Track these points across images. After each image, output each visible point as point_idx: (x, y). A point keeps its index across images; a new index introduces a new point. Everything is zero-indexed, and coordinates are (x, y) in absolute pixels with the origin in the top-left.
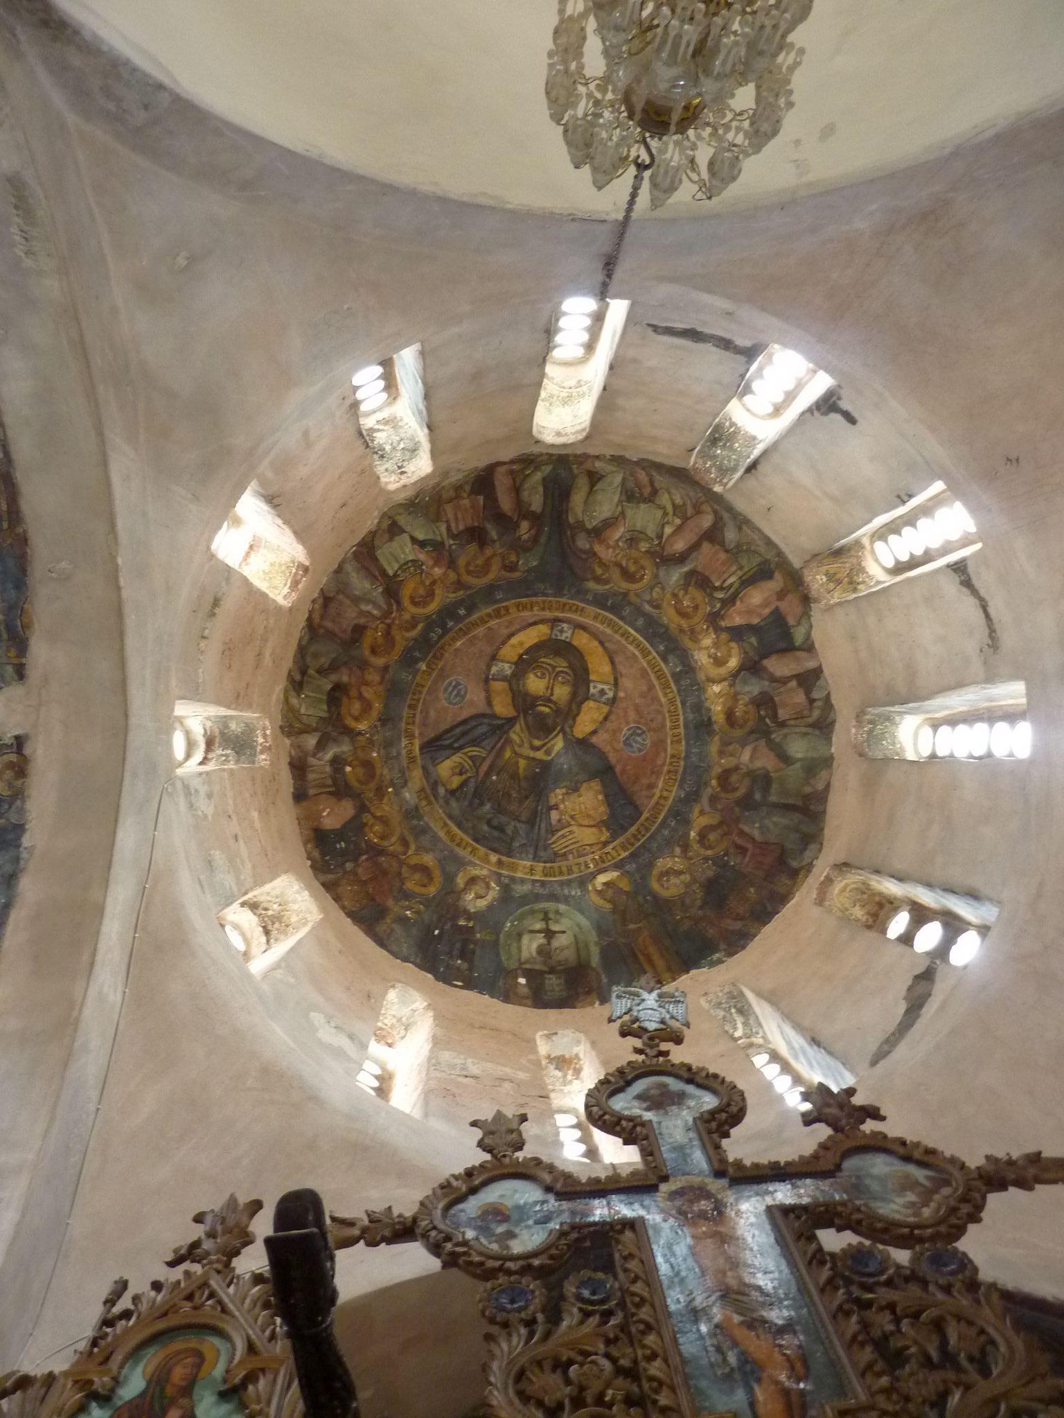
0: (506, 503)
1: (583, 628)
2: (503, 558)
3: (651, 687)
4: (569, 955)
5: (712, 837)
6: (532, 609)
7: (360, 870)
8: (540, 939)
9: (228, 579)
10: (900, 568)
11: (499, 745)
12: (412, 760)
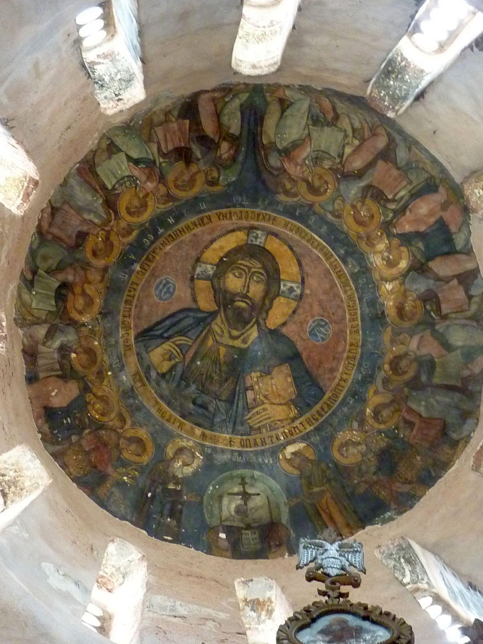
0: (209, 127)
1: (276, 235)
2: (206, 174)
4: (263, 515)
5: (385, 413)
6: (231, 218)
7: (84, 442)
8: (238, 501)
11: (204, 333)
12: (128, 348)
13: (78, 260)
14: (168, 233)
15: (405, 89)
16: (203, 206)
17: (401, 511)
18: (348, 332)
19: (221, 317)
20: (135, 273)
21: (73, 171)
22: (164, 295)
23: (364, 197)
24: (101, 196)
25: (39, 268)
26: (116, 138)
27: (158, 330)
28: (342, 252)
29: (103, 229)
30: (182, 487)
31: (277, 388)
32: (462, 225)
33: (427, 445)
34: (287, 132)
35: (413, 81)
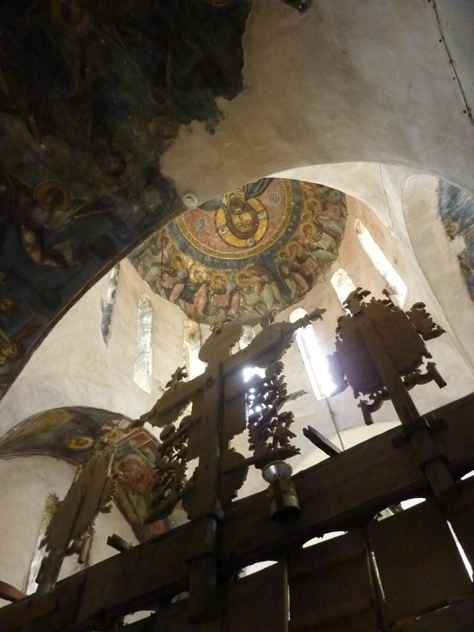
0: (298, 276)
1: (244, 248)
2: (287, 257)
3: (209, 245)
13: (322, 198)
23: (224, 287)
28: (216, 261)
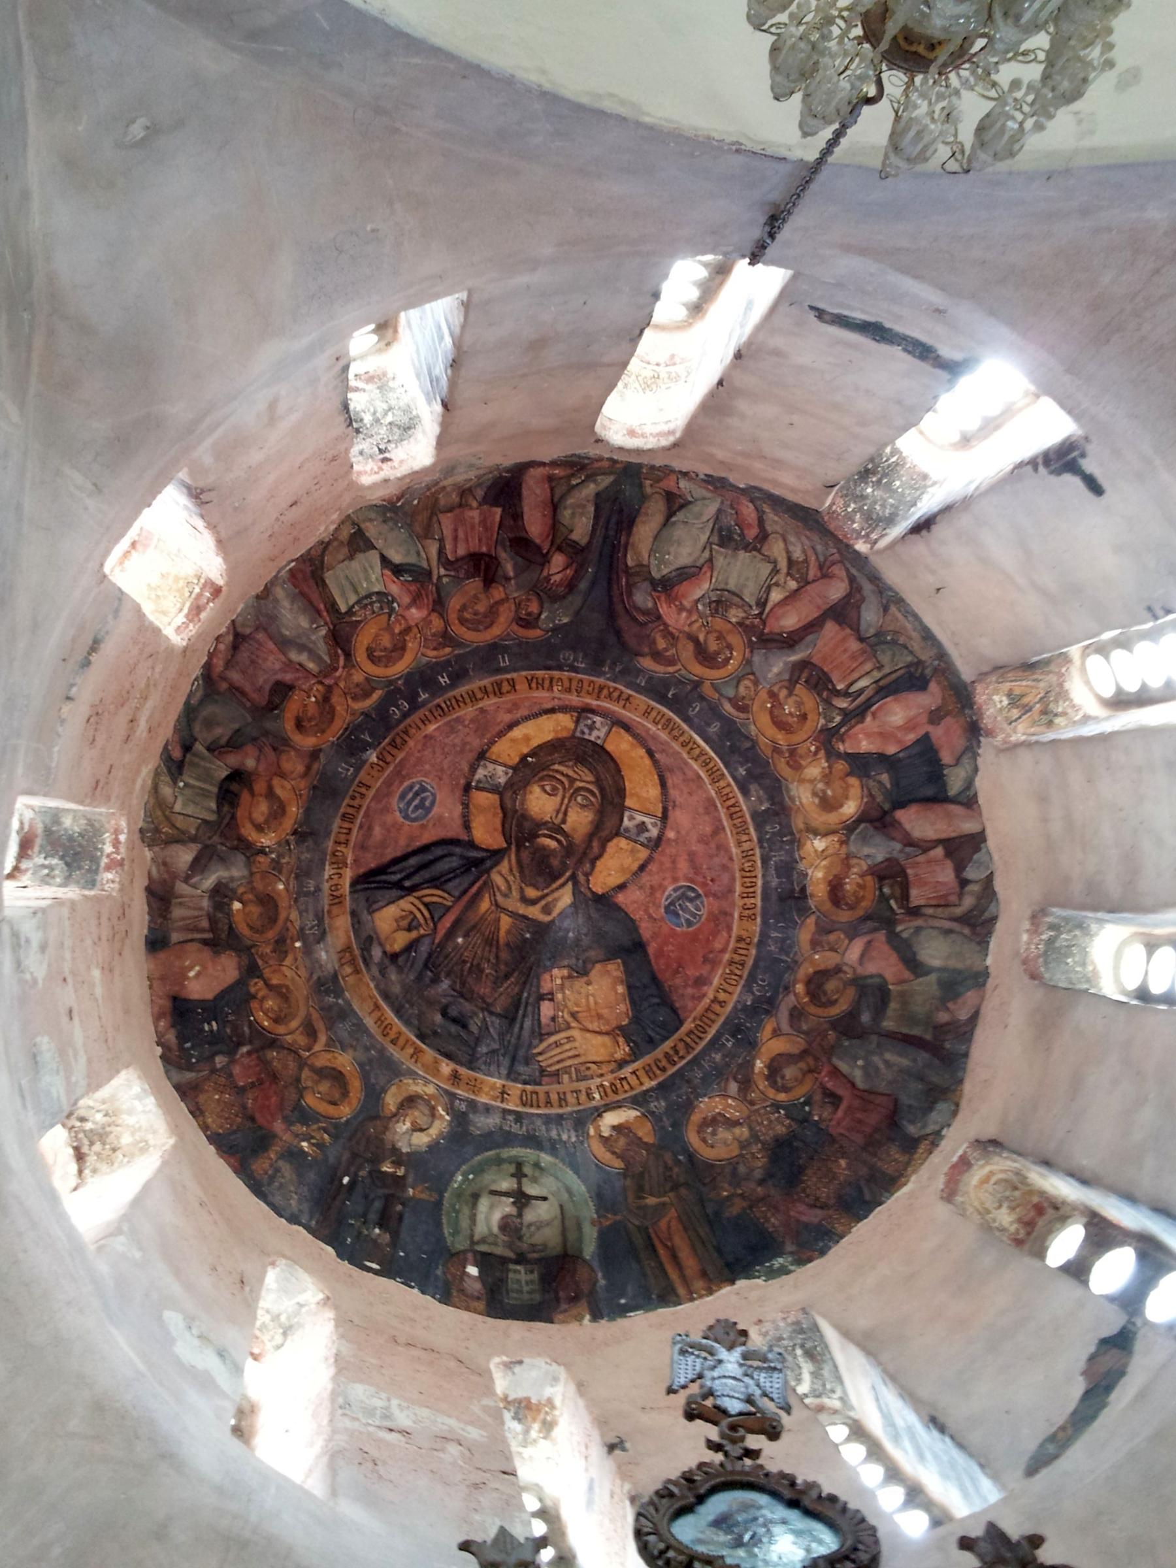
0: (535, 525)
1: (627, 728)
2: (518, 606)
3: (718, 829)
4: (549, 1237)
5: (790, 1072)
6: (551, 688)
7: (237, 1070)
8: (506, 1207)
9: (116, 612)
10: (1121, 702)
11: (474, 889)
12: (337, 900)
13: (266, 733)
14: (435, 702)
15: (892, 505)
16: (504, 661)
17: (804, 1257)
18: (736, 915)
19: (510, 861)
20: (367, 766)
21: (283, 573)
22: (413, 812)
23: (792, 683)
24: (326, 623)
25: (196, 740)
26: (368, 524)
27: (394, 873)
28: (742, 771)
29: (321, 683)
30: (406, 1171)
31: (596, 1003)
32: (963, 753)
33: (859, 1139)
34: (672, 549)
35: (907, 492)
